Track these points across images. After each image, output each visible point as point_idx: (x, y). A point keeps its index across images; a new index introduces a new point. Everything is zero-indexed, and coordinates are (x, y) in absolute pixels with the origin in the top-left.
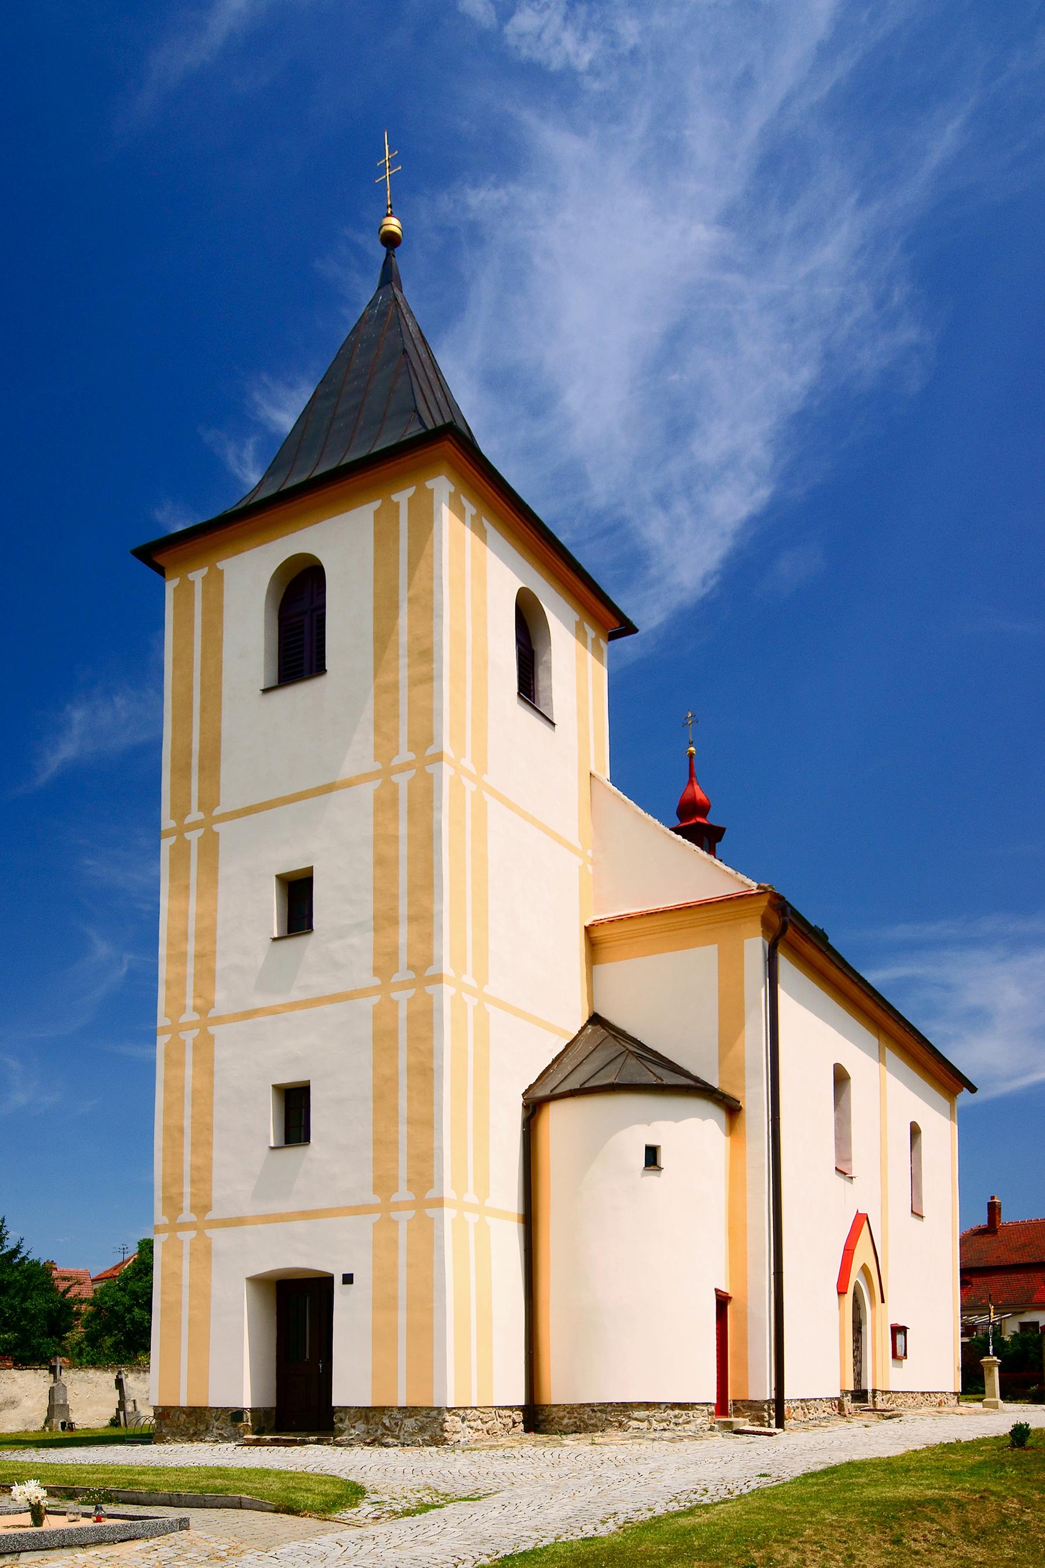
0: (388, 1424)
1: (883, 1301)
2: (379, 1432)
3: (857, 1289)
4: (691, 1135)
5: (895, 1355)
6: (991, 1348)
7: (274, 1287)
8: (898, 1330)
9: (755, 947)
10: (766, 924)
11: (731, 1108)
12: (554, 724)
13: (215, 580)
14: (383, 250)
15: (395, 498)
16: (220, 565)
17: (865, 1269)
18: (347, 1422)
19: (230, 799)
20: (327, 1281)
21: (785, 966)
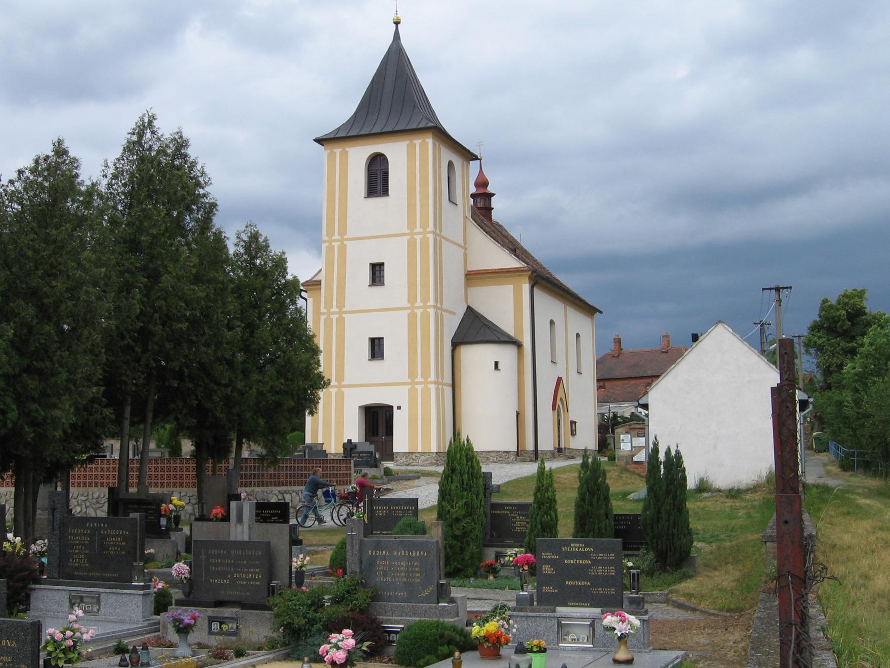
3: (559, 403)
4: (505, 354)
8: (573, 423)
9: (526, 287)
10: (530, 278)
11: (519, 345)
13: (345, 155)
16: (347, 149)
17: (561, 399)
20: (390, 408)
21: (536, 291)
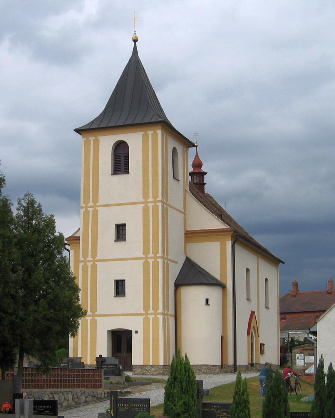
0: (147, 369)
1: (258, 336)
2: (145, 372)
5: (261, 353)
6: (289, 350)
7: (111, 332)
8: (262, 345)
9: (229, 244)
10: (232, 237)
12: (179, 181)
14: (134, 42)
15: (148, 132)
16: (99, 138)
17: (254, 327)
18: (136, 369)
19: (102, 200)
